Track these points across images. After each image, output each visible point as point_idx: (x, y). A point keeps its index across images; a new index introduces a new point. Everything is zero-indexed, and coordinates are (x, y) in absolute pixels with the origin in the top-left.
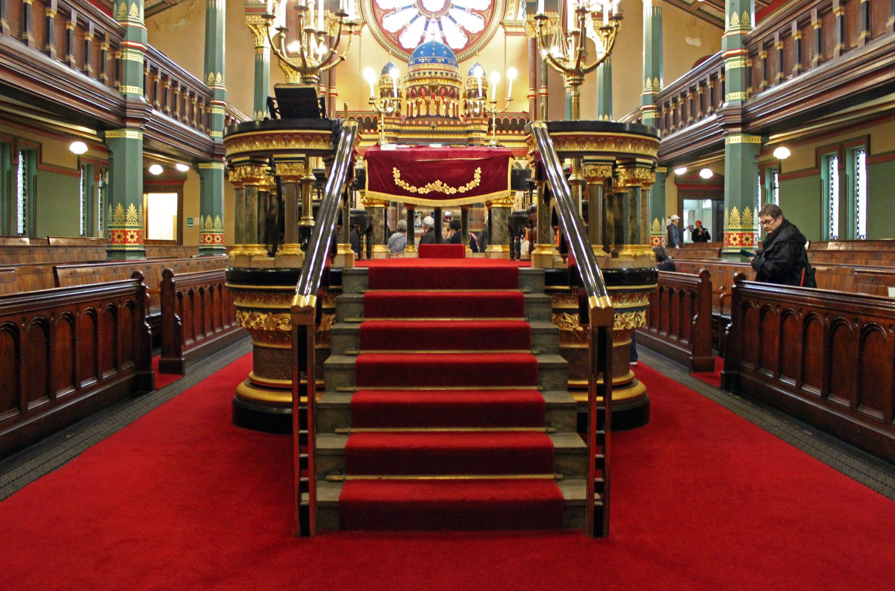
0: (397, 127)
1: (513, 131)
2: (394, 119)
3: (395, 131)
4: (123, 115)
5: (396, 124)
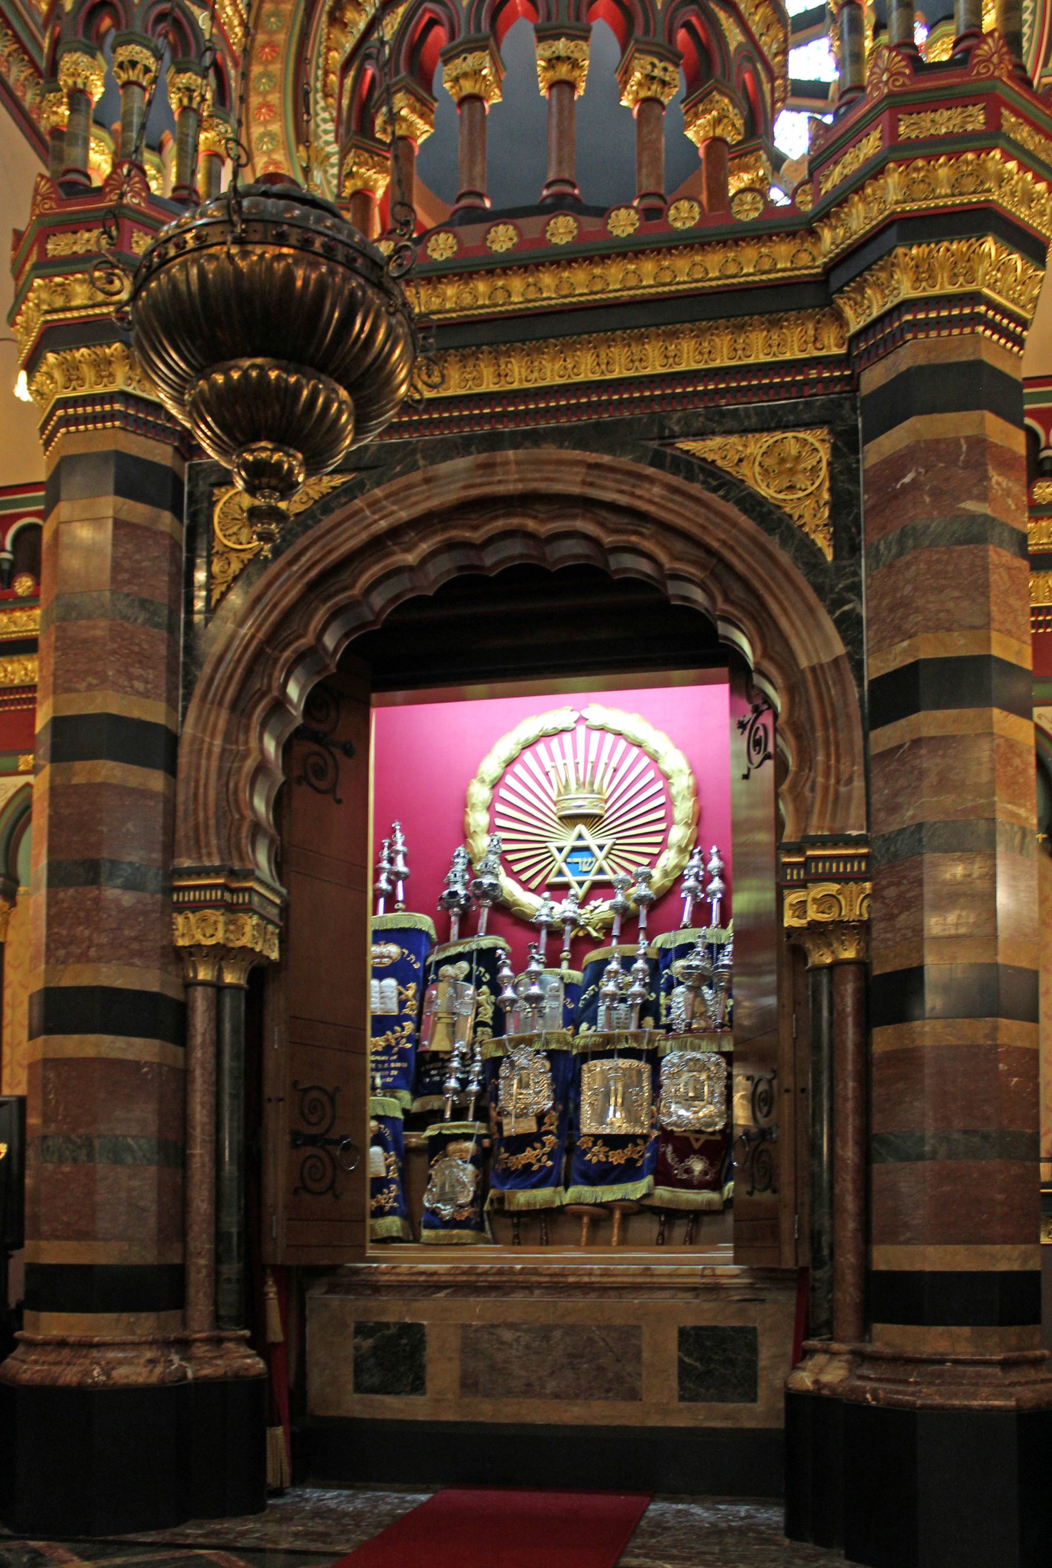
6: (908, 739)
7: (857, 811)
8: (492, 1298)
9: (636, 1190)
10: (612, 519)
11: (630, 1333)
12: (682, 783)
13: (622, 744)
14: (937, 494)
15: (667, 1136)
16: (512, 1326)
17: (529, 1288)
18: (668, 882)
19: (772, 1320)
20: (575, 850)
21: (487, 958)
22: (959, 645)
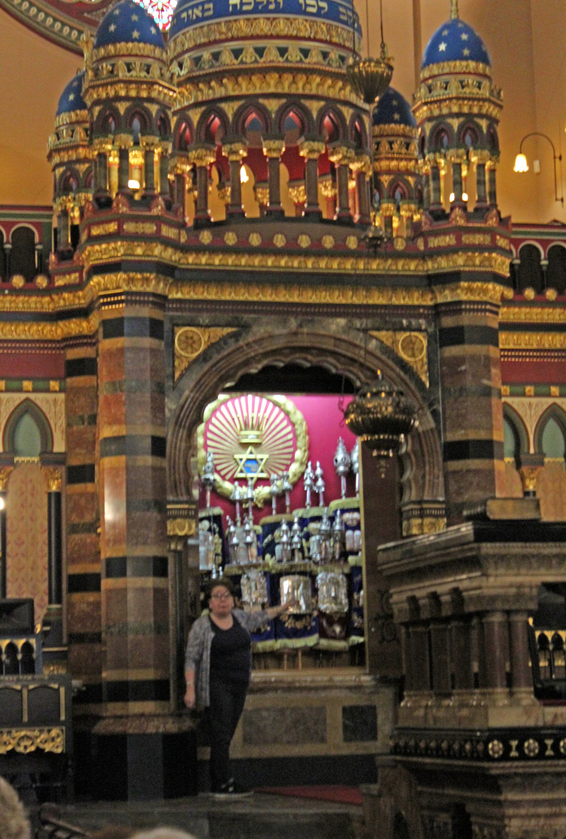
0: (169, 255)
1: (540, 291)
2: (157, 220)
3: (166, 270)
4: (153, 83)
5: (167, 243)
6: (465, 469)
7: (441, 490)
8: (258, 696)
9: (311, 641)
10: (342, 359)
11: (321, 710)
12: (301, 429)
13: (277, 410)
14: (474, 376)
15: (322, 614)
16: (268, 710)
17: (276, 689)
18: (295, 479)
19: (383, 700)
20: (248, 460)
21: (217, 519)
22: (482, 435)
